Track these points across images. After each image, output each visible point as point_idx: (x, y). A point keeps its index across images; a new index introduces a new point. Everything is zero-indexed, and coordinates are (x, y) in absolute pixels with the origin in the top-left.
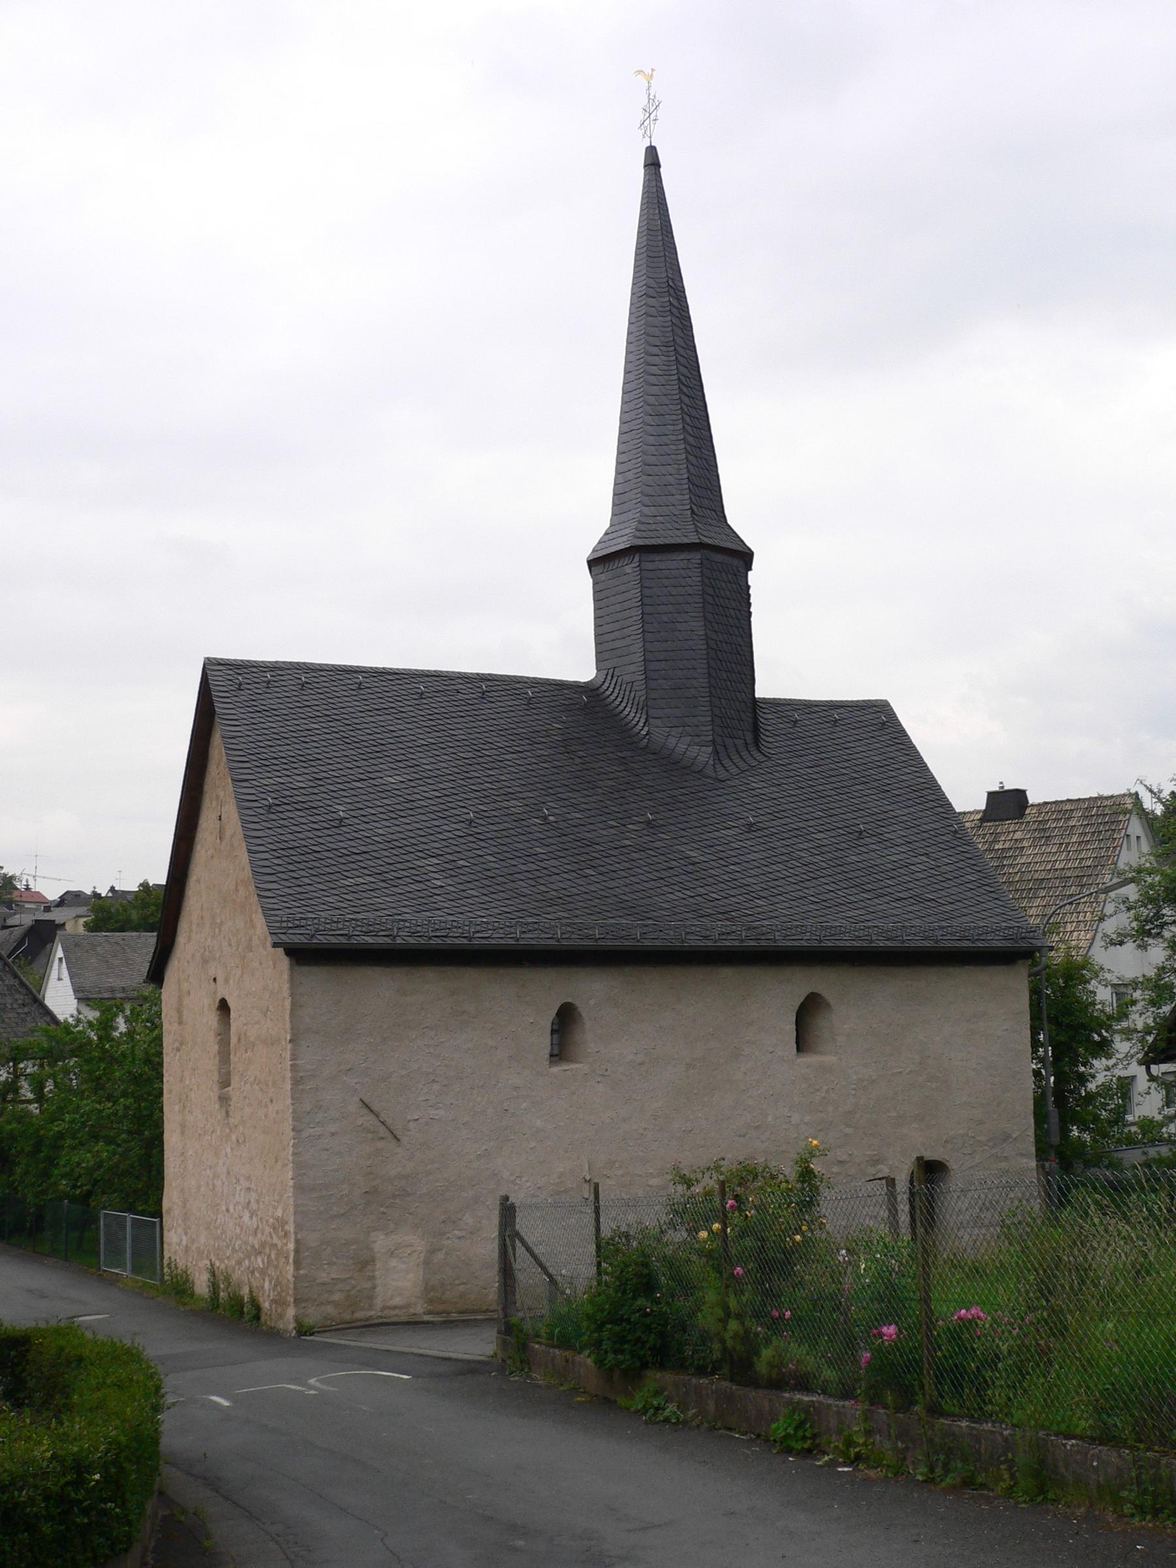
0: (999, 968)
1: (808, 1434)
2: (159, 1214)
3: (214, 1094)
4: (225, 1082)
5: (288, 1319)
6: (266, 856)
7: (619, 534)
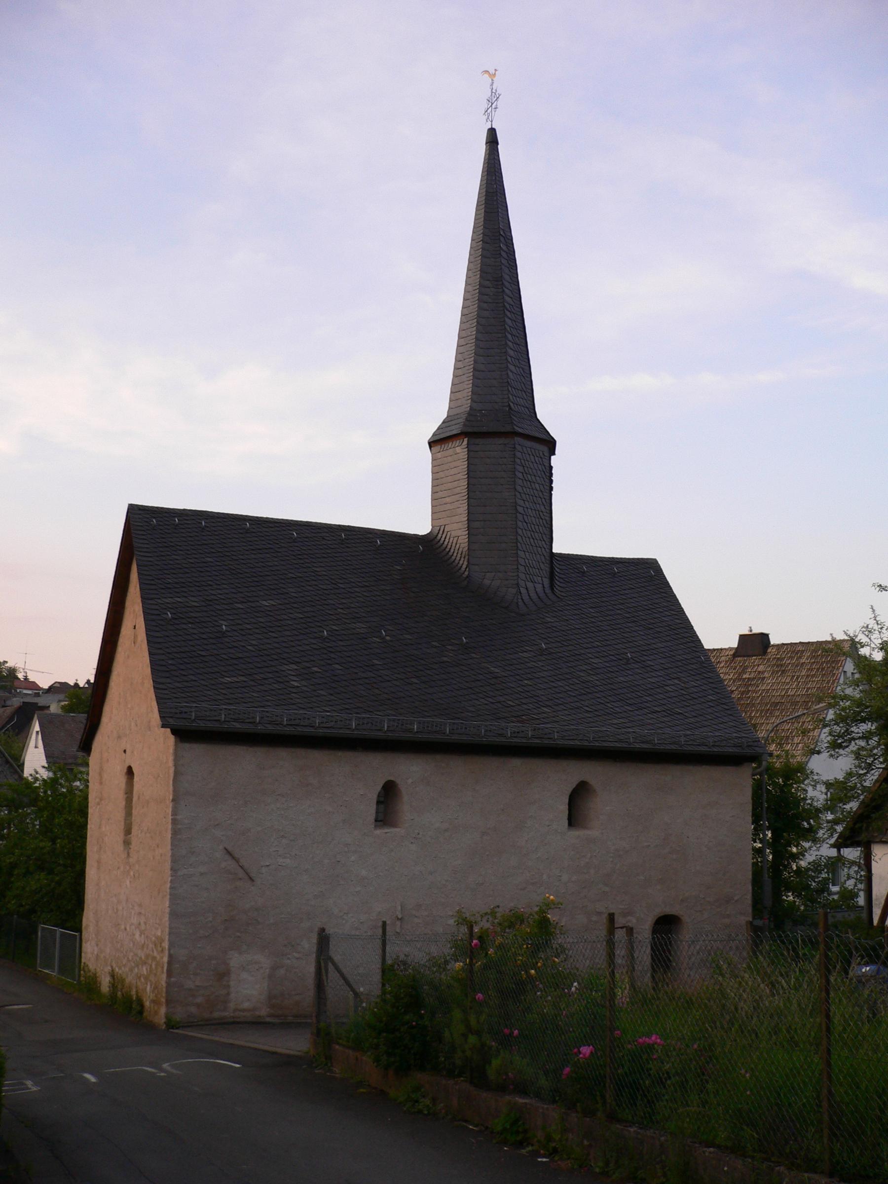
0: (730, 768)
1: (520, 1130)
2: (79, 930)
3: (120, 838)
4: (128, 831)
5: (160, 1015)
6: (163, 657)
7: (453, 423)
